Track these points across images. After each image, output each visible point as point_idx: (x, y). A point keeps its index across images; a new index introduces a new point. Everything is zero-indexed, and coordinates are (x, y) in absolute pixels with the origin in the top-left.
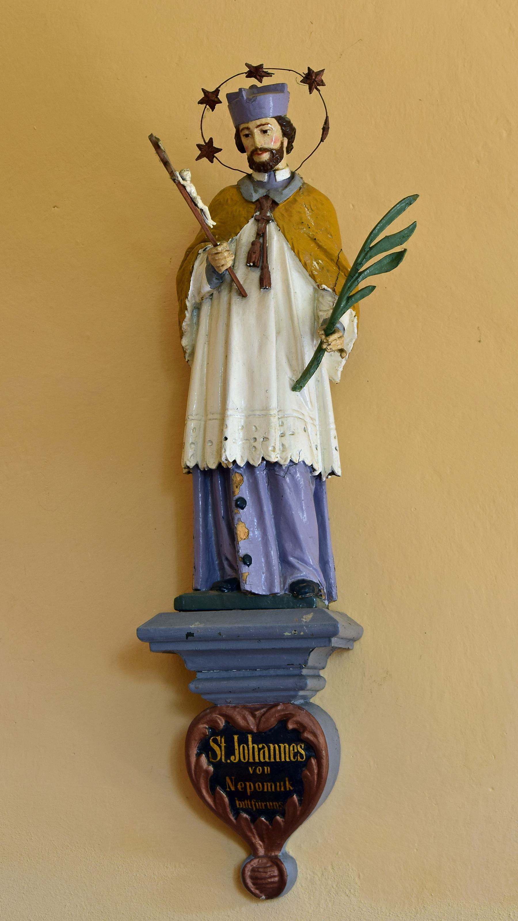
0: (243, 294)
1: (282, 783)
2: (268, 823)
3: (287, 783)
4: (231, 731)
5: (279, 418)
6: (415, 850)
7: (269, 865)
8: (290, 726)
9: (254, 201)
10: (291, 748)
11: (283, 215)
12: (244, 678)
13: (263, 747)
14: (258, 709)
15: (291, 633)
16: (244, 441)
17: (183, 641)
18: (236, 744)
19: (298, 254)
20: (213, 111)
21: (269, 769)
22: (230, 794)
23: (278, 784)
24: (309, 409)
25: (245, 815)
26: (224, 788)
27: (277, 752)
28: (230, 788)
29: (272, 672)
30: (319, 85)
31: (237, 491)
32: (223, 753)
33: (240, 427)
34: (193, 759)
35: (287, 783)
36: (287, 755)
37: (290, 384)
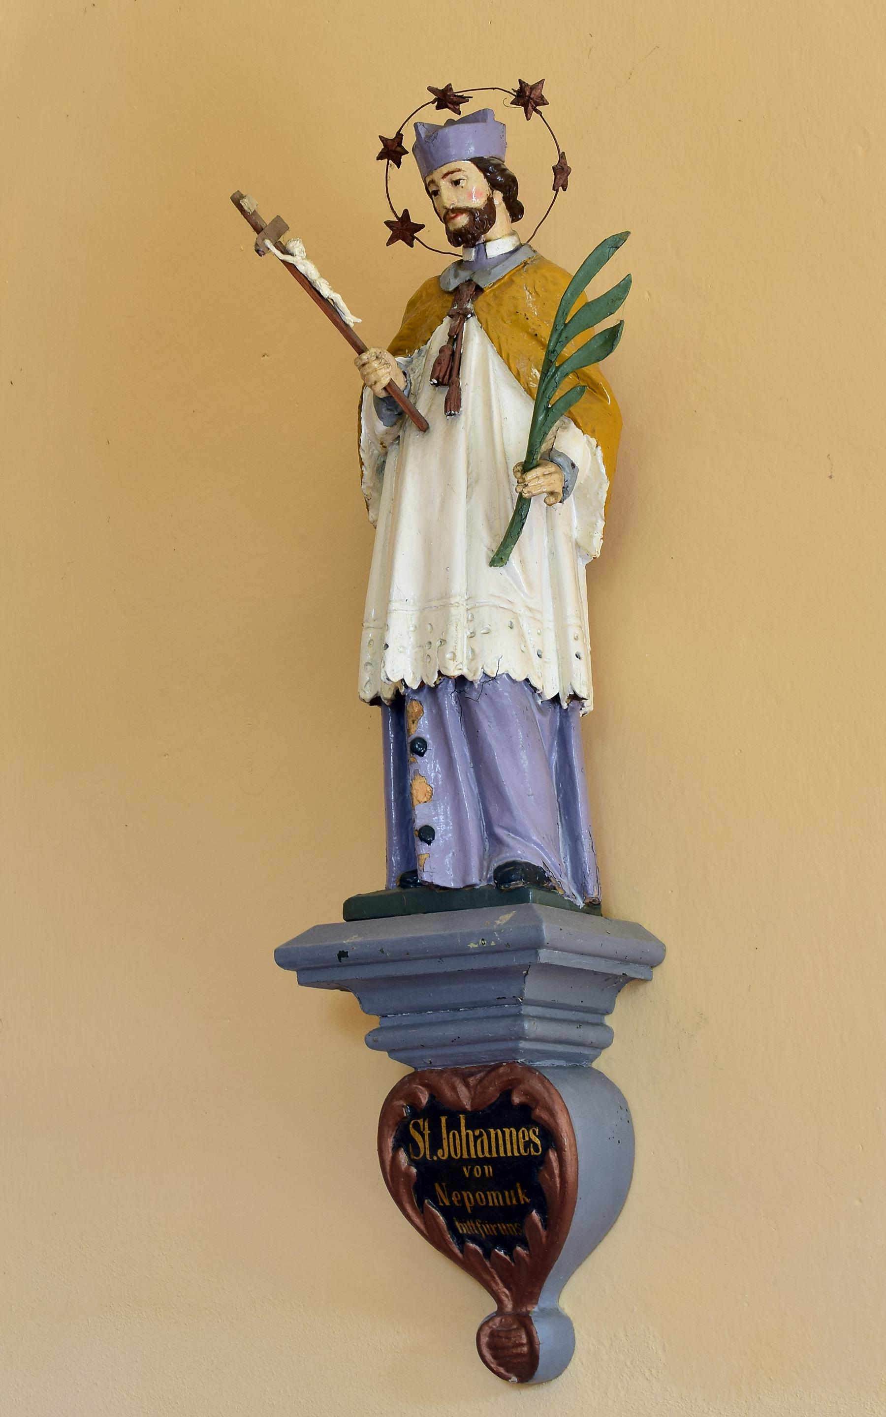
0: (423, 427)
1: (512, 1193)
2: (507, 1258)
3: (519, 1191)
4: (438, 1112)
5: (468, 610)
6: (746, 1305)
7: (515, 1327)
8: (516, 1100)
9: (451, 289)
10: (521, 1135)
11: (488, 304)
12: (445, 1022)
13: (481, 1135)
14: (472, 1074)
15: (478, 943)
16: (417, 649)
17: (333, 967)
18: (444, 1131)
19: (508, 359)
20: (399, 167)
21: (491, 1170)
22: (443, 1210)
23: (507, 1193)
24: (525, 594)
25: (472, 1245)
26: (435, 1201)
27: (501, 1142)
28: (443, 1202)
29: (480, 1012)
30: (539, 105)
31: (413, 728)
32: (427, 1146)
33: (412, 629)
34: (388, 1156)
35: (519, 1191)
36: (515, 1147)
37: (488, 556)
